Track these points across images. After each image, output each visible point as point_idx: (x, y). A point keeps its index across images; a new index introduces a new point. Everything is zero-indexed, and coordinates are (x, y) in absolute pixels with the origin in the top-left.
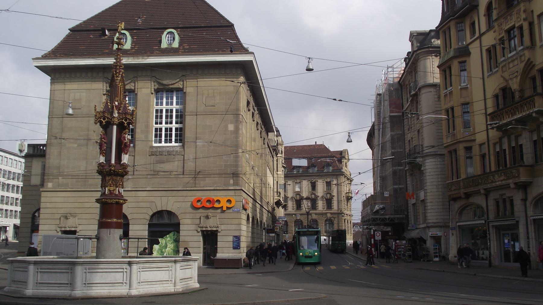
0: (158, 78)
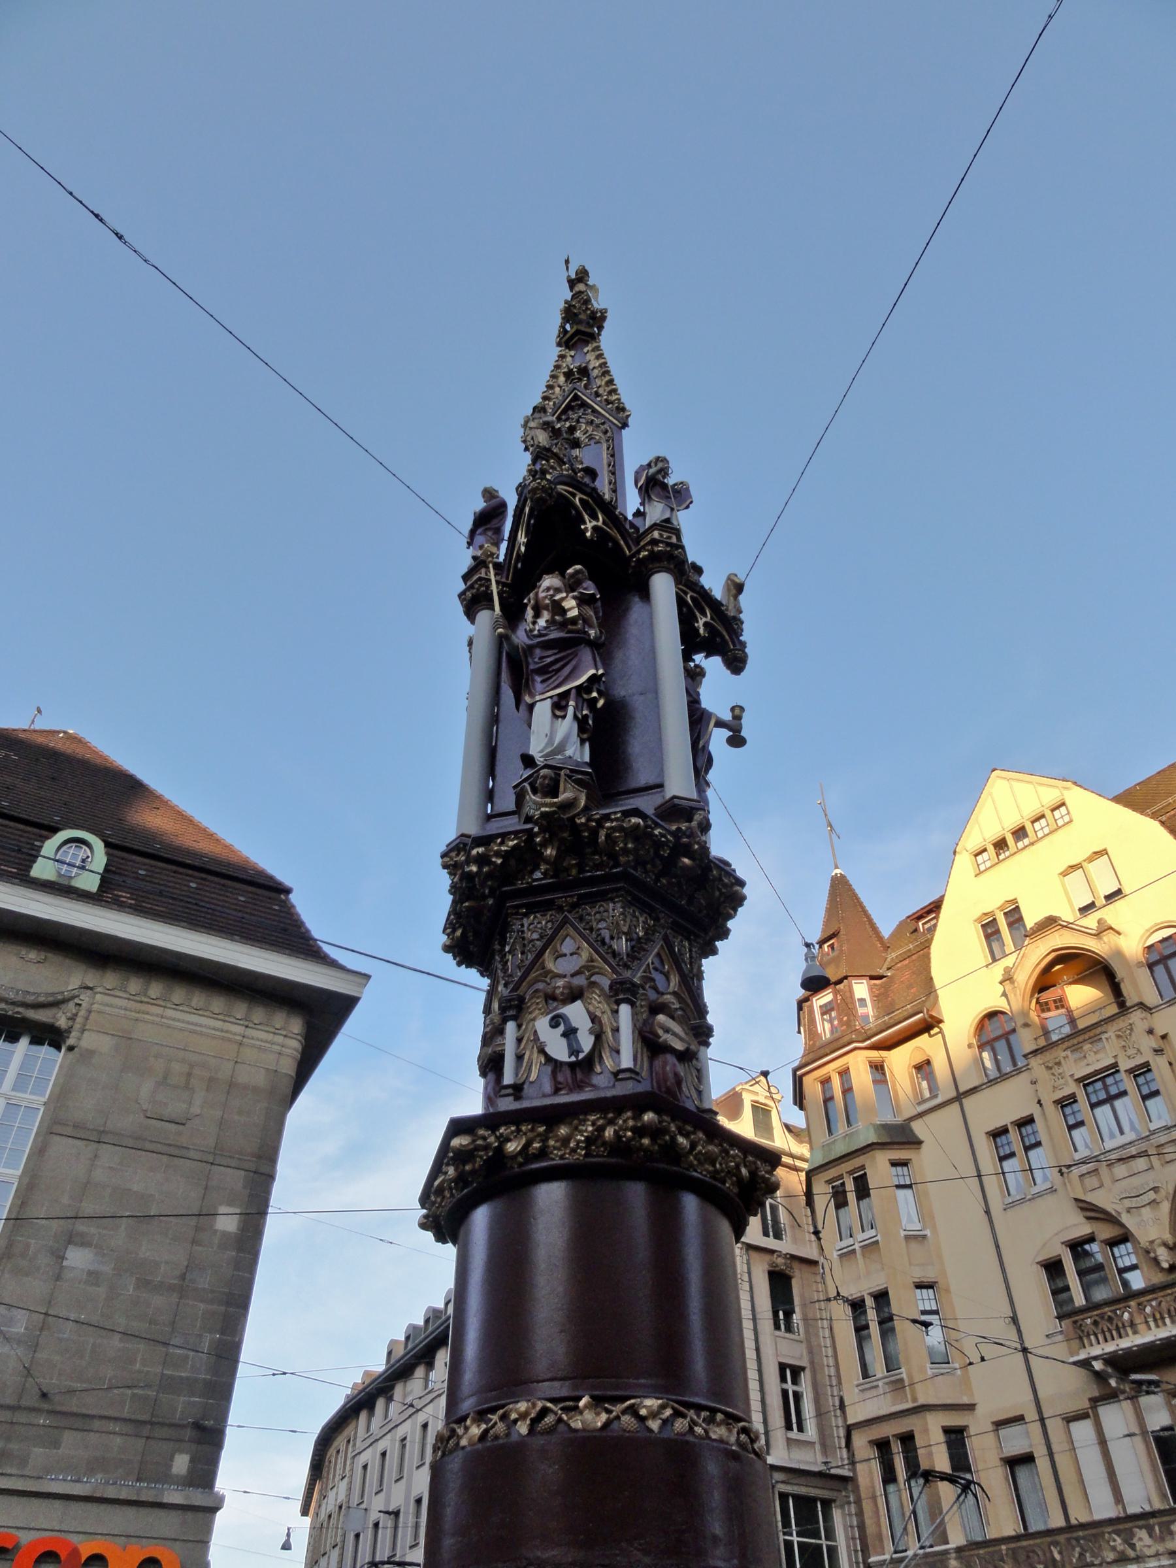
0: (32, 1309)
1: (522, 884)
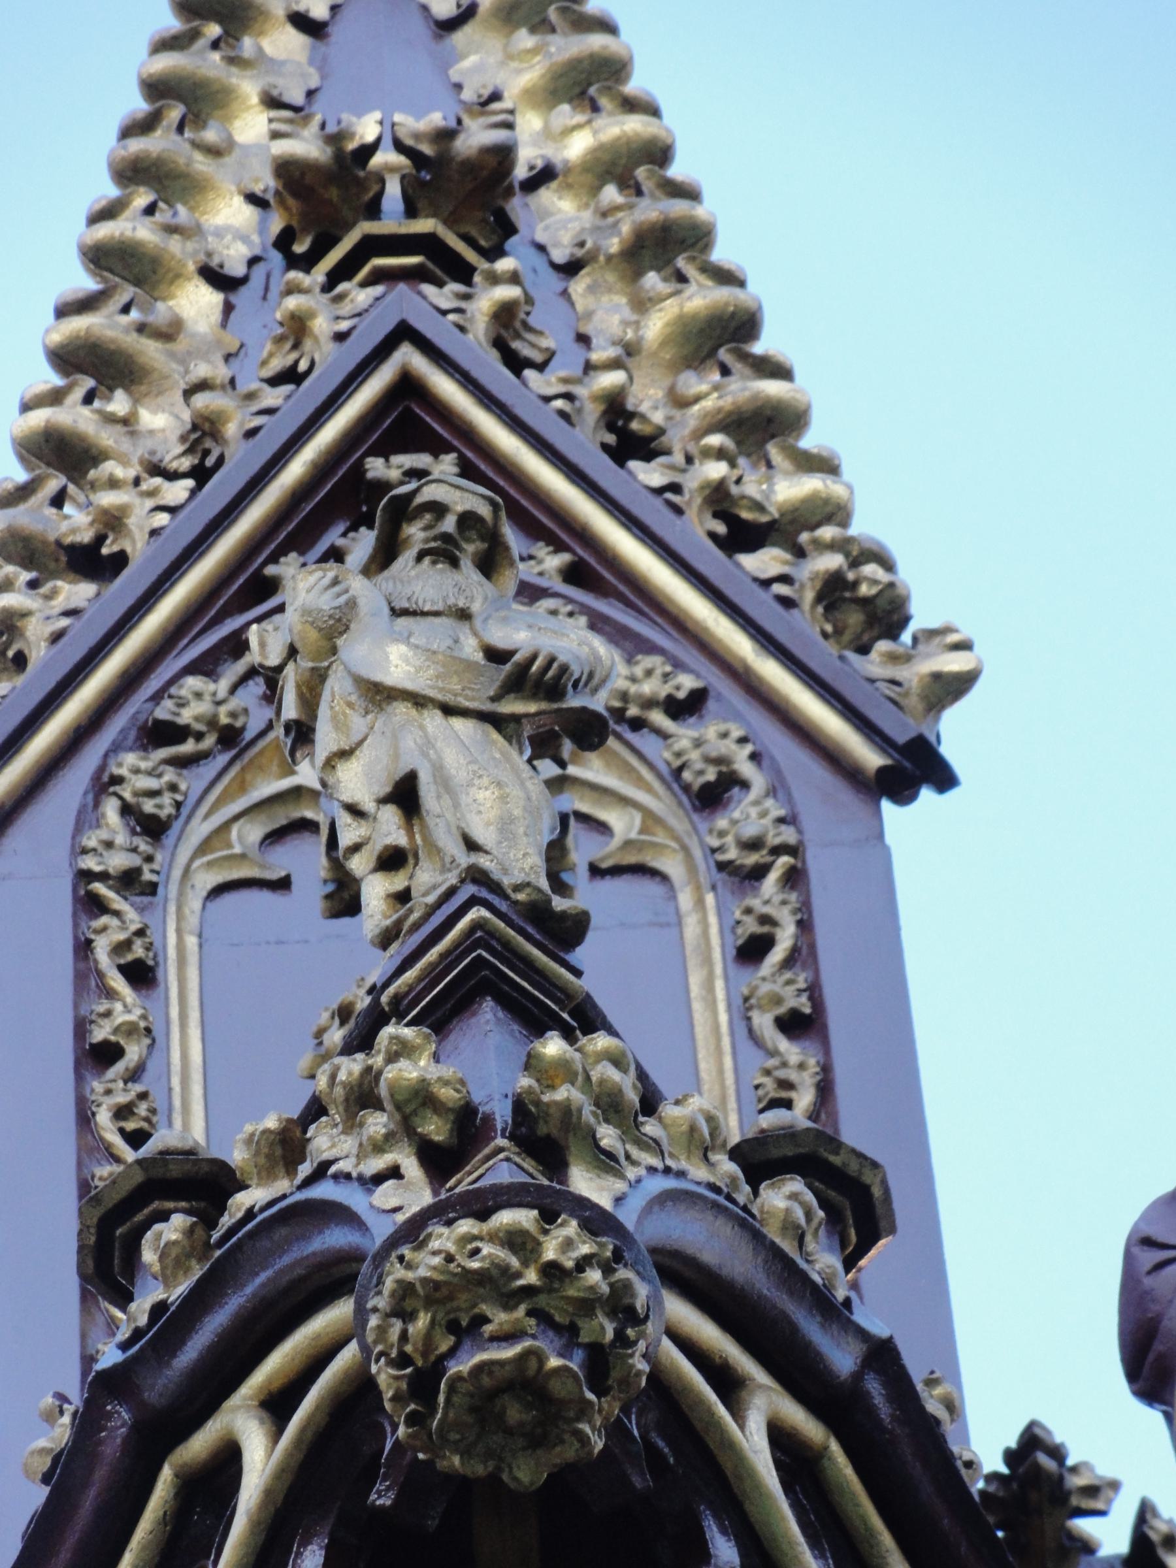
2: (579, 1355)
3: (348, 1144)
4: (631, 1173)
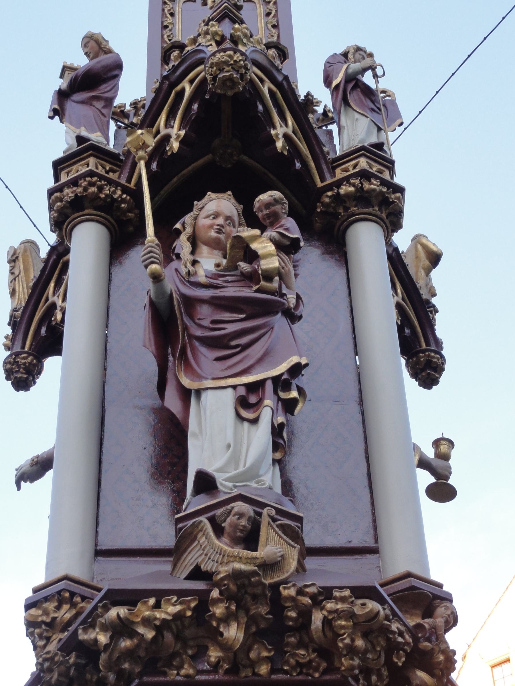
1: (178, 674)
2: (239, 75)
3: (204, 40)
4: (248, 47)
